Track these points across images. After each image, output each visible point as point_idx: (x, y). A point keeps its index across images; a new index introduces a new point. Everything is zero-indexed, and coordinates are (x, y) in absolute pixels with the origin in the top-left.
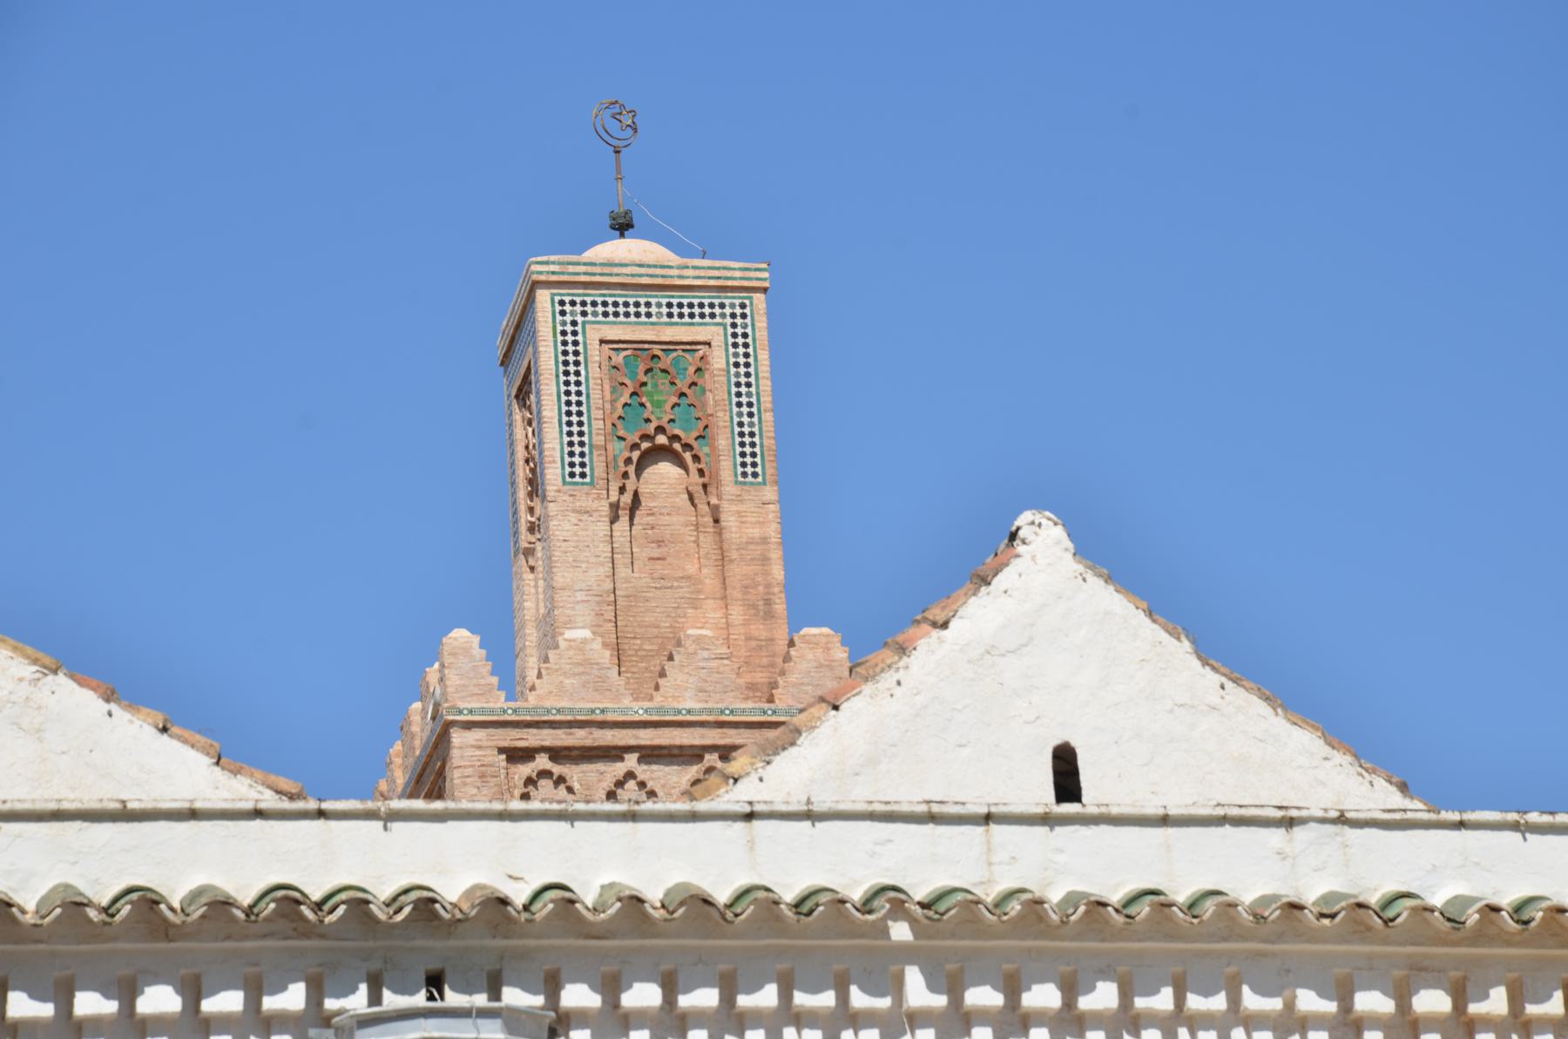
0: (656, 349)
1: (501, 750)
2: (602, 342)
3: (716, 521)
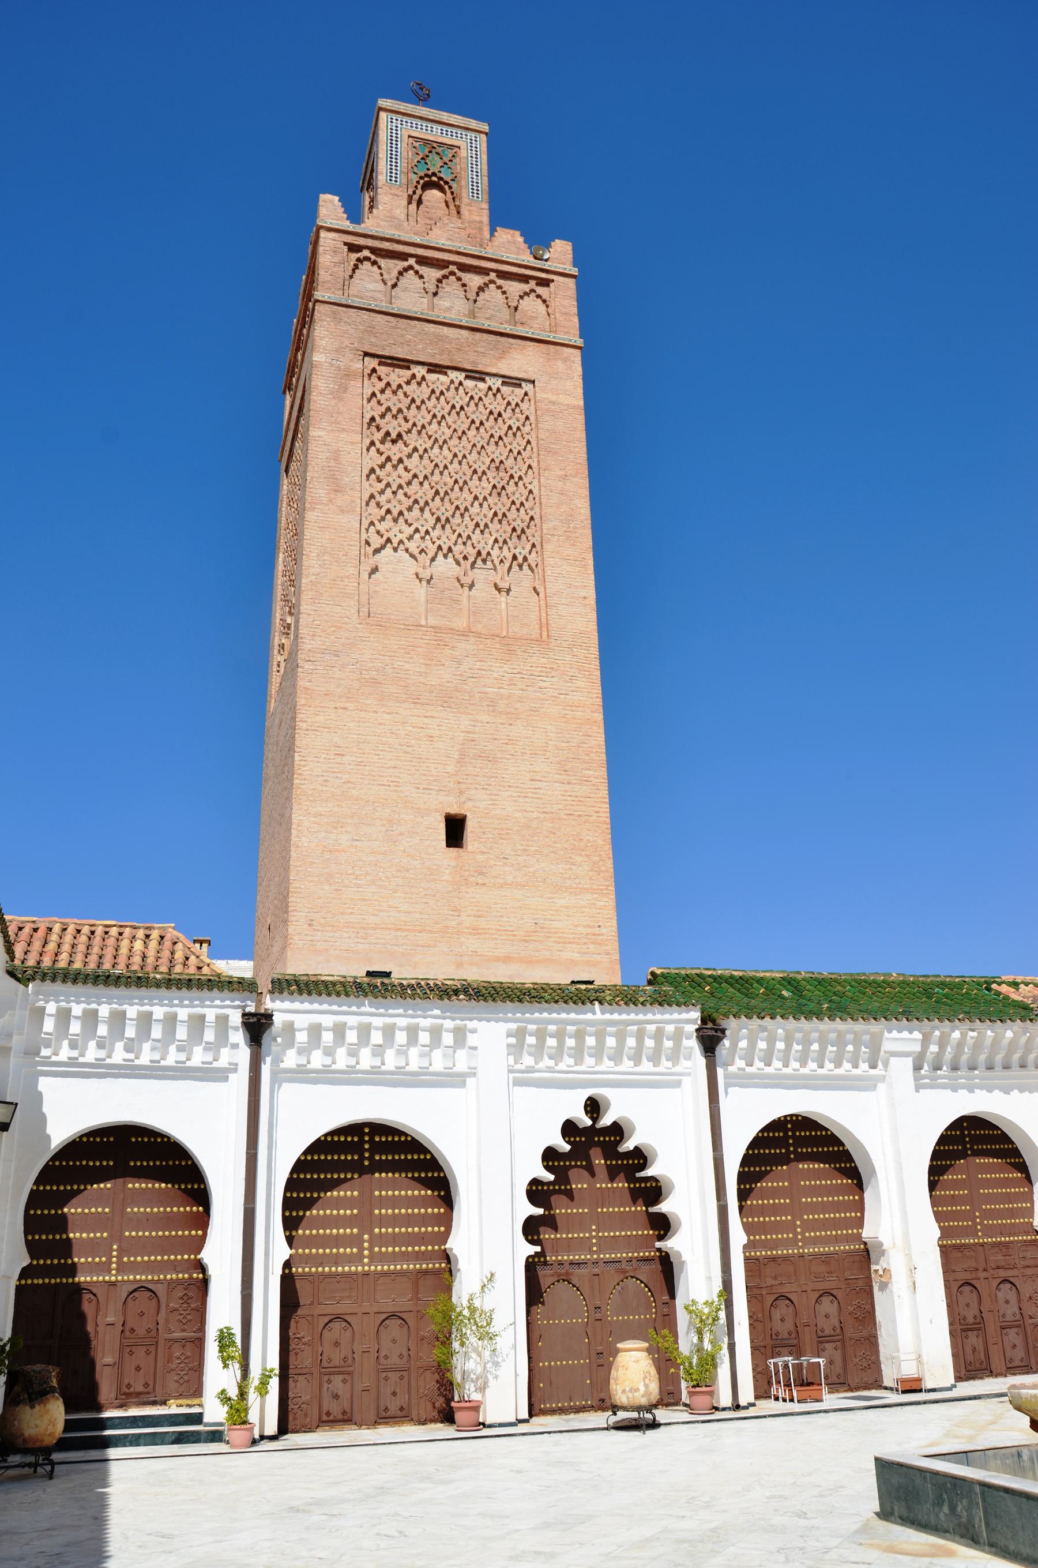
0: (435, 145)
1: (345, 244)
2: (409, 136)
3: (458, 213)
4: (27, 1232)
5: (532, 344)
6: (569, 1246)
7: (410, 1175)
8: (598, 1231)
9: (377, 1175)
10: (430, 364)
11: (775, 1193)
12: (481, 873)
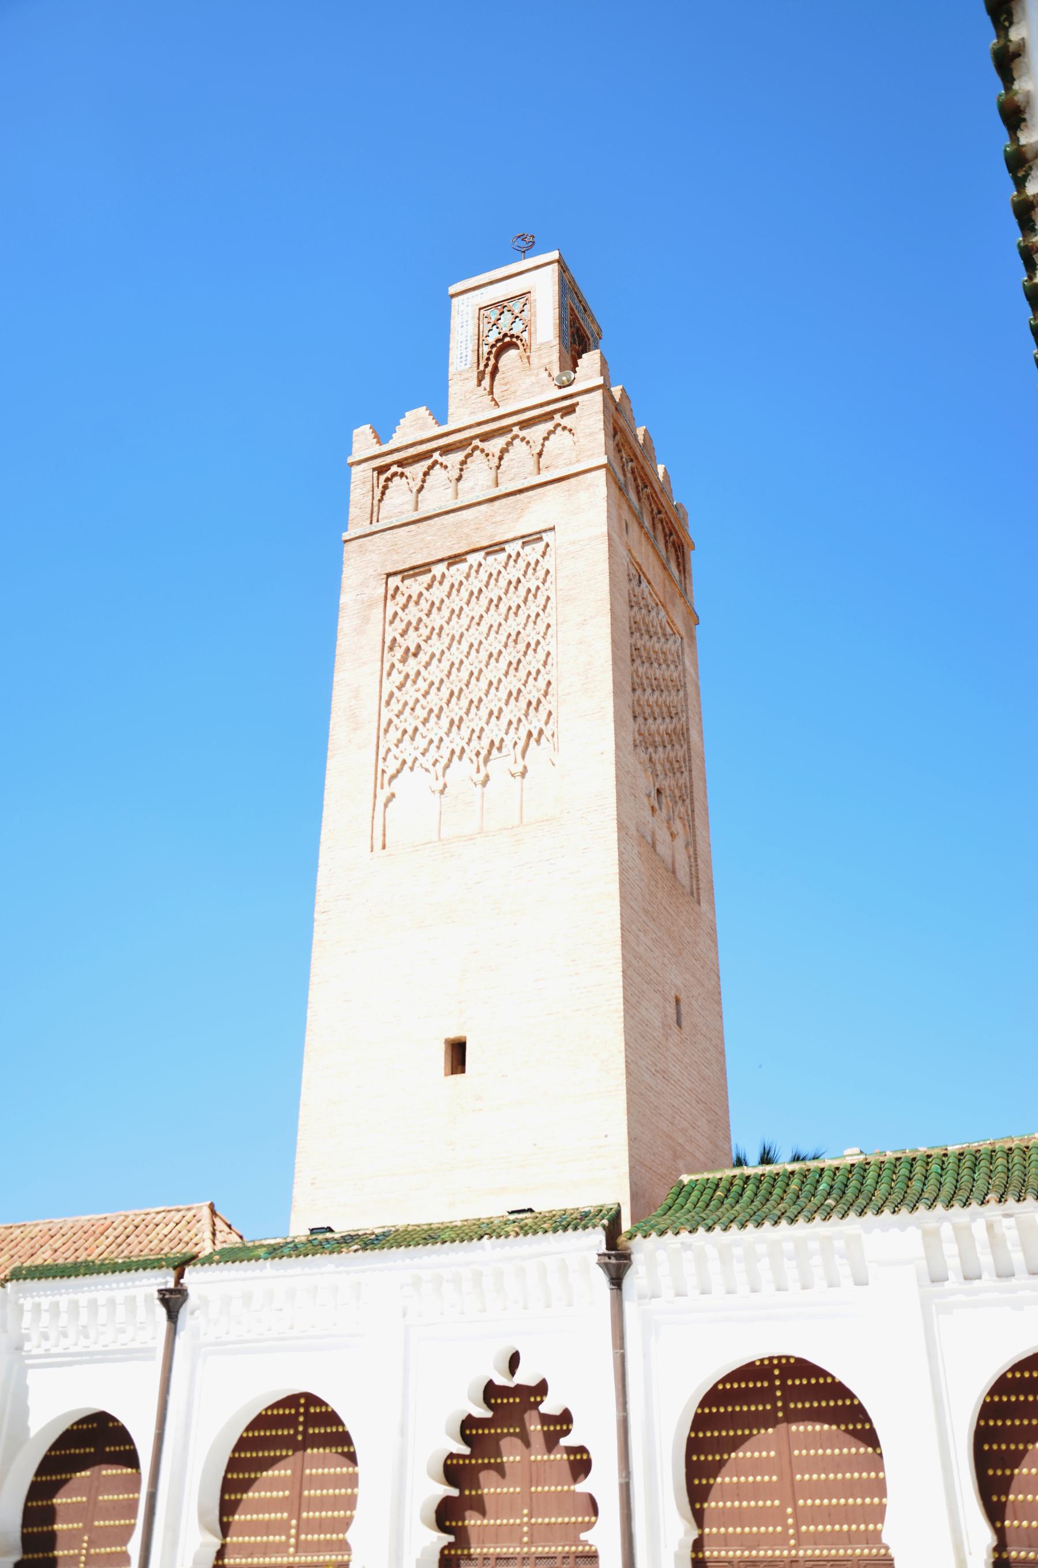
4: (25, 1524)
6: (497, 1535)
7: (851, 1427)
8: (530, 1516)
9: (309, 1451)
10: (450, 558)
11: (756, 1468)
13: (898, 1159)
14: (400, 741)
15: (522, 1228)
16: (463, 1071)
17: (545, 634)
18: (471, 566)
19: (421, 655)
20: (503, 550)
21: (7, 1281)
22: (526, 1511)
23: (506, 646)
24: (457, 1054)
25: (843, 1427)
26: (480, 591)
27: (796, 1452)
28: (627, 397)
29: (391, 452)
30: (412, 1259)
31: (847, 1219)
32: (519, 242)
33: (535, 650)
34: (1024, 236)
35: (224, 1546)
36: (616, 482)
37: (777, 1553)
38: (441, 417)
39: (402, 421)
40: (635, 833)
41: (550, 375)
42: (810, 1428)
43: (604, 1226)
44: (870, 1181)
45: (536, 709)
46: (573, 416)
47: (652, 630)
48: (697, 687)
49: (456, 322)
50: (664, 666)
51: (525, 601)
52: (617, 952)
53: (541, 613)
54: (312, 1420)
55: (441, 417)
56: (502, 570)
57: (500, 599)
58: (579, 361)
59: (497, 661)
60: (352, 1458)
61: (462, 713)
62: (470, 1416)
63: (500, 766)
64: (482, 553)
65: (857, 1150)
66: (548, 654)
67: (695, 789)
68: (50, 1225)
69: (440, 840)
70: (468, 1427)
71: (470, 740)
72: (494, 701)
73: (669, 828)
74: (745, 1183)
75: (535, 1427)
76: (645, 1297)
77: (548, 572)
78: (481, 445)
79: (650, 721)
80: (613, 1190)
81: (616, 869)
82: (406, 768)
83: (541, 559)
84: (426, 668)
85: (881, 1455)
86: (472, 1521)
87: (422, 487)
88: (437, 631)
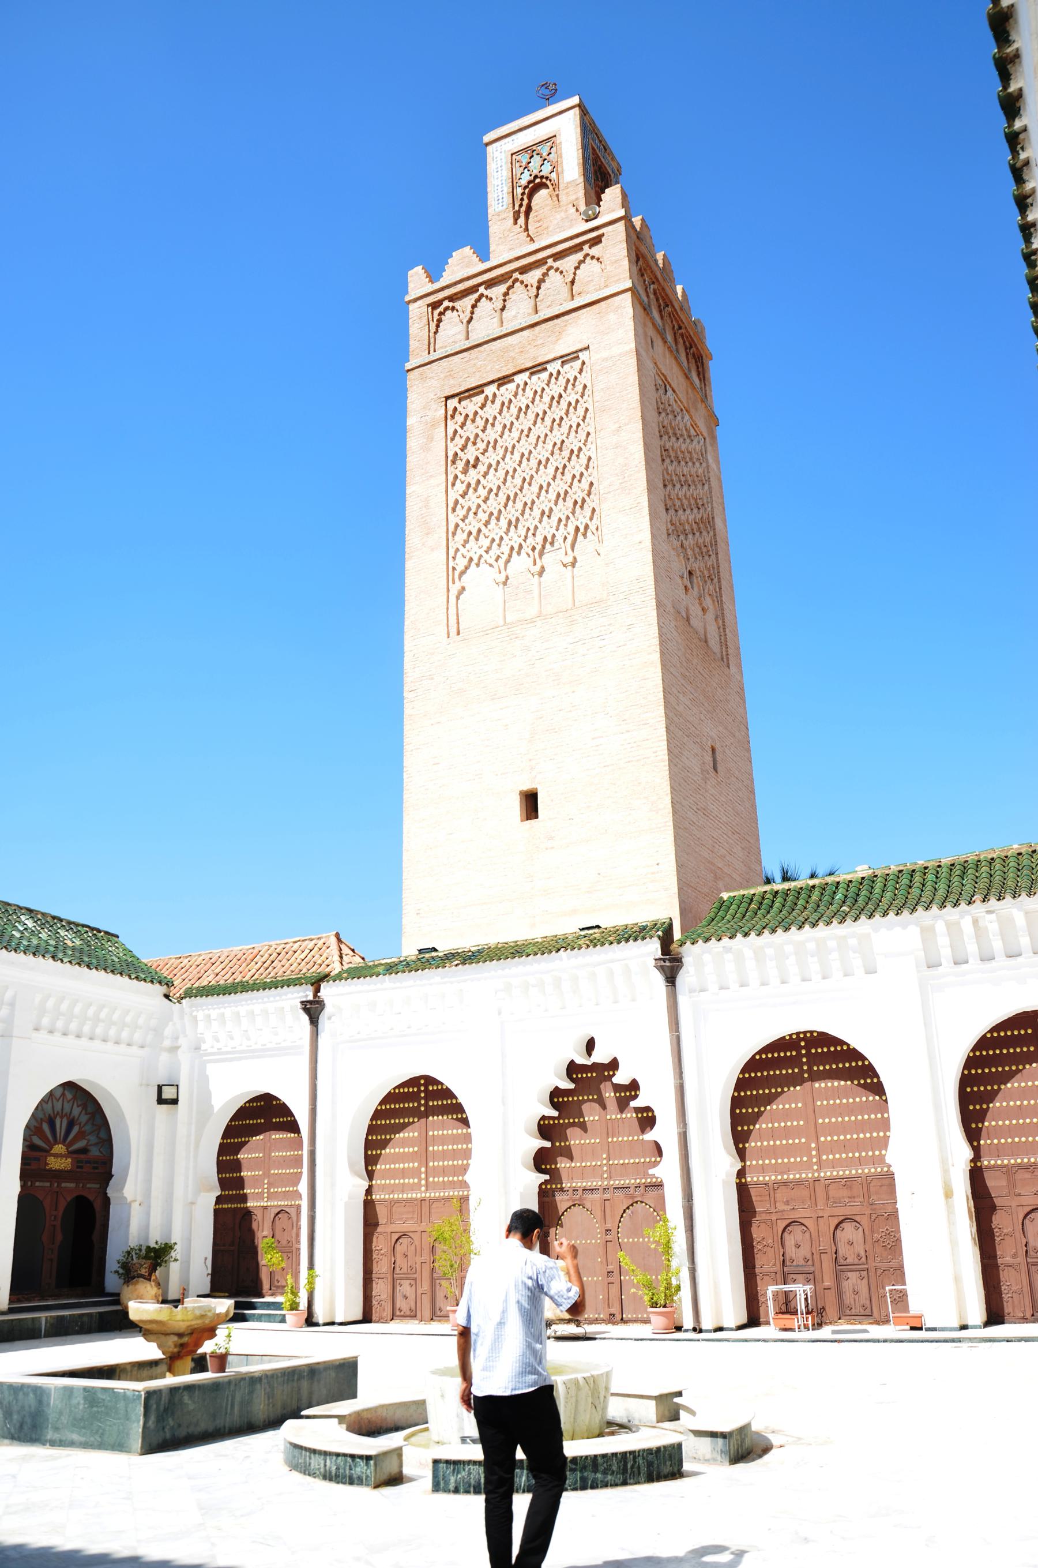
4: (219, 1171)
5: (585, 310)
7: (862, 1082)
9: (431, 1118)
10: (499, 379)
11: (787, 1115)
12: (551, 838)
13: (900, 871)
14: (466, 542)
15: (591, 941)
16: (536, 817)
17: (586, 441)
18: (518, 386)
19: (480, 466)
20: (546, 369)
21: (182, 998)
22: (604, 1156)
23: (552, 454)
24: (531, 803)
25: (856, 1082)
26: (528, 407)
27: (819, 1103)
28: (647, 226)
29: (442, 289)
30: (503, 969)
31: (859, 922)
32: (543, 90)
33: (578, 456)
34: (999, 48)
35: (370, 1187)
36: (641, 303)
37: (804, 1176)
38: (483, 254)
39: (450, 261)
40: (672, 610)
41: (577, 210)
42: (829, 1084)
43: (659, 937)
44: (877, 890)
45: (582, 507)
46: (600, 246)
47: (678, 432)
48: (720, 480)
49: (492, 167)
50: (690, 464)
51: (567, 413)
52: (661, 711)
53: (581, 423)
54: (430, 1095)
55: (483, 254)
56: (546, 387)
57: (545, 413)
58: (603, 196)
59: (546, 467)
60: (465, 1122)
61: (518, 514)
62: (557, 1087)
63: (552, 559)
64: (527, 374)
65: (866, 867)
66: (590, 458)
67: (721, 569)
68: (210, 956)
69: (505, 624)
70: (556, 1096)
71: (526, 537)
72: (545, 503)
73: (701, 604)
74: (775, 897)
75: (609, 1094)
76: (695, 991)
77: (585, 387)
78: (521, 277)
79: (680, 512)
80: (664, 905)
81: (656, 641)
82: (473, 564)
83: (578, 375)
84: (484, 477)
85: (886, 1101)
86: (563, 1164)
87: (471, 318)
88: (492, 444)
